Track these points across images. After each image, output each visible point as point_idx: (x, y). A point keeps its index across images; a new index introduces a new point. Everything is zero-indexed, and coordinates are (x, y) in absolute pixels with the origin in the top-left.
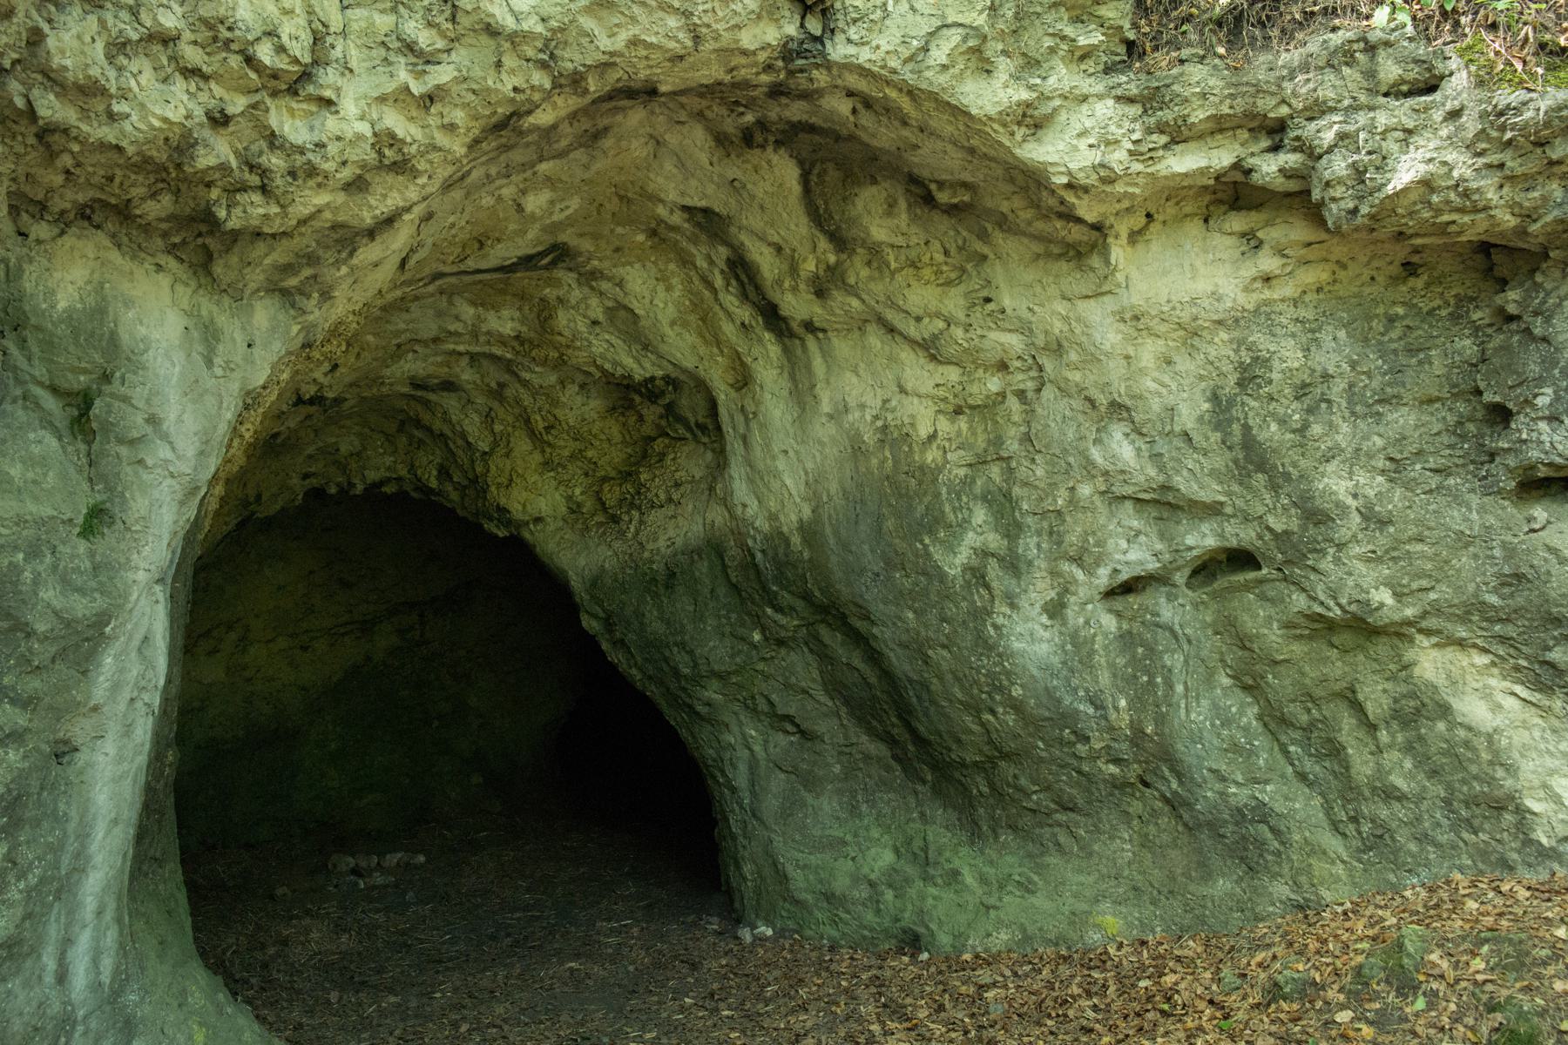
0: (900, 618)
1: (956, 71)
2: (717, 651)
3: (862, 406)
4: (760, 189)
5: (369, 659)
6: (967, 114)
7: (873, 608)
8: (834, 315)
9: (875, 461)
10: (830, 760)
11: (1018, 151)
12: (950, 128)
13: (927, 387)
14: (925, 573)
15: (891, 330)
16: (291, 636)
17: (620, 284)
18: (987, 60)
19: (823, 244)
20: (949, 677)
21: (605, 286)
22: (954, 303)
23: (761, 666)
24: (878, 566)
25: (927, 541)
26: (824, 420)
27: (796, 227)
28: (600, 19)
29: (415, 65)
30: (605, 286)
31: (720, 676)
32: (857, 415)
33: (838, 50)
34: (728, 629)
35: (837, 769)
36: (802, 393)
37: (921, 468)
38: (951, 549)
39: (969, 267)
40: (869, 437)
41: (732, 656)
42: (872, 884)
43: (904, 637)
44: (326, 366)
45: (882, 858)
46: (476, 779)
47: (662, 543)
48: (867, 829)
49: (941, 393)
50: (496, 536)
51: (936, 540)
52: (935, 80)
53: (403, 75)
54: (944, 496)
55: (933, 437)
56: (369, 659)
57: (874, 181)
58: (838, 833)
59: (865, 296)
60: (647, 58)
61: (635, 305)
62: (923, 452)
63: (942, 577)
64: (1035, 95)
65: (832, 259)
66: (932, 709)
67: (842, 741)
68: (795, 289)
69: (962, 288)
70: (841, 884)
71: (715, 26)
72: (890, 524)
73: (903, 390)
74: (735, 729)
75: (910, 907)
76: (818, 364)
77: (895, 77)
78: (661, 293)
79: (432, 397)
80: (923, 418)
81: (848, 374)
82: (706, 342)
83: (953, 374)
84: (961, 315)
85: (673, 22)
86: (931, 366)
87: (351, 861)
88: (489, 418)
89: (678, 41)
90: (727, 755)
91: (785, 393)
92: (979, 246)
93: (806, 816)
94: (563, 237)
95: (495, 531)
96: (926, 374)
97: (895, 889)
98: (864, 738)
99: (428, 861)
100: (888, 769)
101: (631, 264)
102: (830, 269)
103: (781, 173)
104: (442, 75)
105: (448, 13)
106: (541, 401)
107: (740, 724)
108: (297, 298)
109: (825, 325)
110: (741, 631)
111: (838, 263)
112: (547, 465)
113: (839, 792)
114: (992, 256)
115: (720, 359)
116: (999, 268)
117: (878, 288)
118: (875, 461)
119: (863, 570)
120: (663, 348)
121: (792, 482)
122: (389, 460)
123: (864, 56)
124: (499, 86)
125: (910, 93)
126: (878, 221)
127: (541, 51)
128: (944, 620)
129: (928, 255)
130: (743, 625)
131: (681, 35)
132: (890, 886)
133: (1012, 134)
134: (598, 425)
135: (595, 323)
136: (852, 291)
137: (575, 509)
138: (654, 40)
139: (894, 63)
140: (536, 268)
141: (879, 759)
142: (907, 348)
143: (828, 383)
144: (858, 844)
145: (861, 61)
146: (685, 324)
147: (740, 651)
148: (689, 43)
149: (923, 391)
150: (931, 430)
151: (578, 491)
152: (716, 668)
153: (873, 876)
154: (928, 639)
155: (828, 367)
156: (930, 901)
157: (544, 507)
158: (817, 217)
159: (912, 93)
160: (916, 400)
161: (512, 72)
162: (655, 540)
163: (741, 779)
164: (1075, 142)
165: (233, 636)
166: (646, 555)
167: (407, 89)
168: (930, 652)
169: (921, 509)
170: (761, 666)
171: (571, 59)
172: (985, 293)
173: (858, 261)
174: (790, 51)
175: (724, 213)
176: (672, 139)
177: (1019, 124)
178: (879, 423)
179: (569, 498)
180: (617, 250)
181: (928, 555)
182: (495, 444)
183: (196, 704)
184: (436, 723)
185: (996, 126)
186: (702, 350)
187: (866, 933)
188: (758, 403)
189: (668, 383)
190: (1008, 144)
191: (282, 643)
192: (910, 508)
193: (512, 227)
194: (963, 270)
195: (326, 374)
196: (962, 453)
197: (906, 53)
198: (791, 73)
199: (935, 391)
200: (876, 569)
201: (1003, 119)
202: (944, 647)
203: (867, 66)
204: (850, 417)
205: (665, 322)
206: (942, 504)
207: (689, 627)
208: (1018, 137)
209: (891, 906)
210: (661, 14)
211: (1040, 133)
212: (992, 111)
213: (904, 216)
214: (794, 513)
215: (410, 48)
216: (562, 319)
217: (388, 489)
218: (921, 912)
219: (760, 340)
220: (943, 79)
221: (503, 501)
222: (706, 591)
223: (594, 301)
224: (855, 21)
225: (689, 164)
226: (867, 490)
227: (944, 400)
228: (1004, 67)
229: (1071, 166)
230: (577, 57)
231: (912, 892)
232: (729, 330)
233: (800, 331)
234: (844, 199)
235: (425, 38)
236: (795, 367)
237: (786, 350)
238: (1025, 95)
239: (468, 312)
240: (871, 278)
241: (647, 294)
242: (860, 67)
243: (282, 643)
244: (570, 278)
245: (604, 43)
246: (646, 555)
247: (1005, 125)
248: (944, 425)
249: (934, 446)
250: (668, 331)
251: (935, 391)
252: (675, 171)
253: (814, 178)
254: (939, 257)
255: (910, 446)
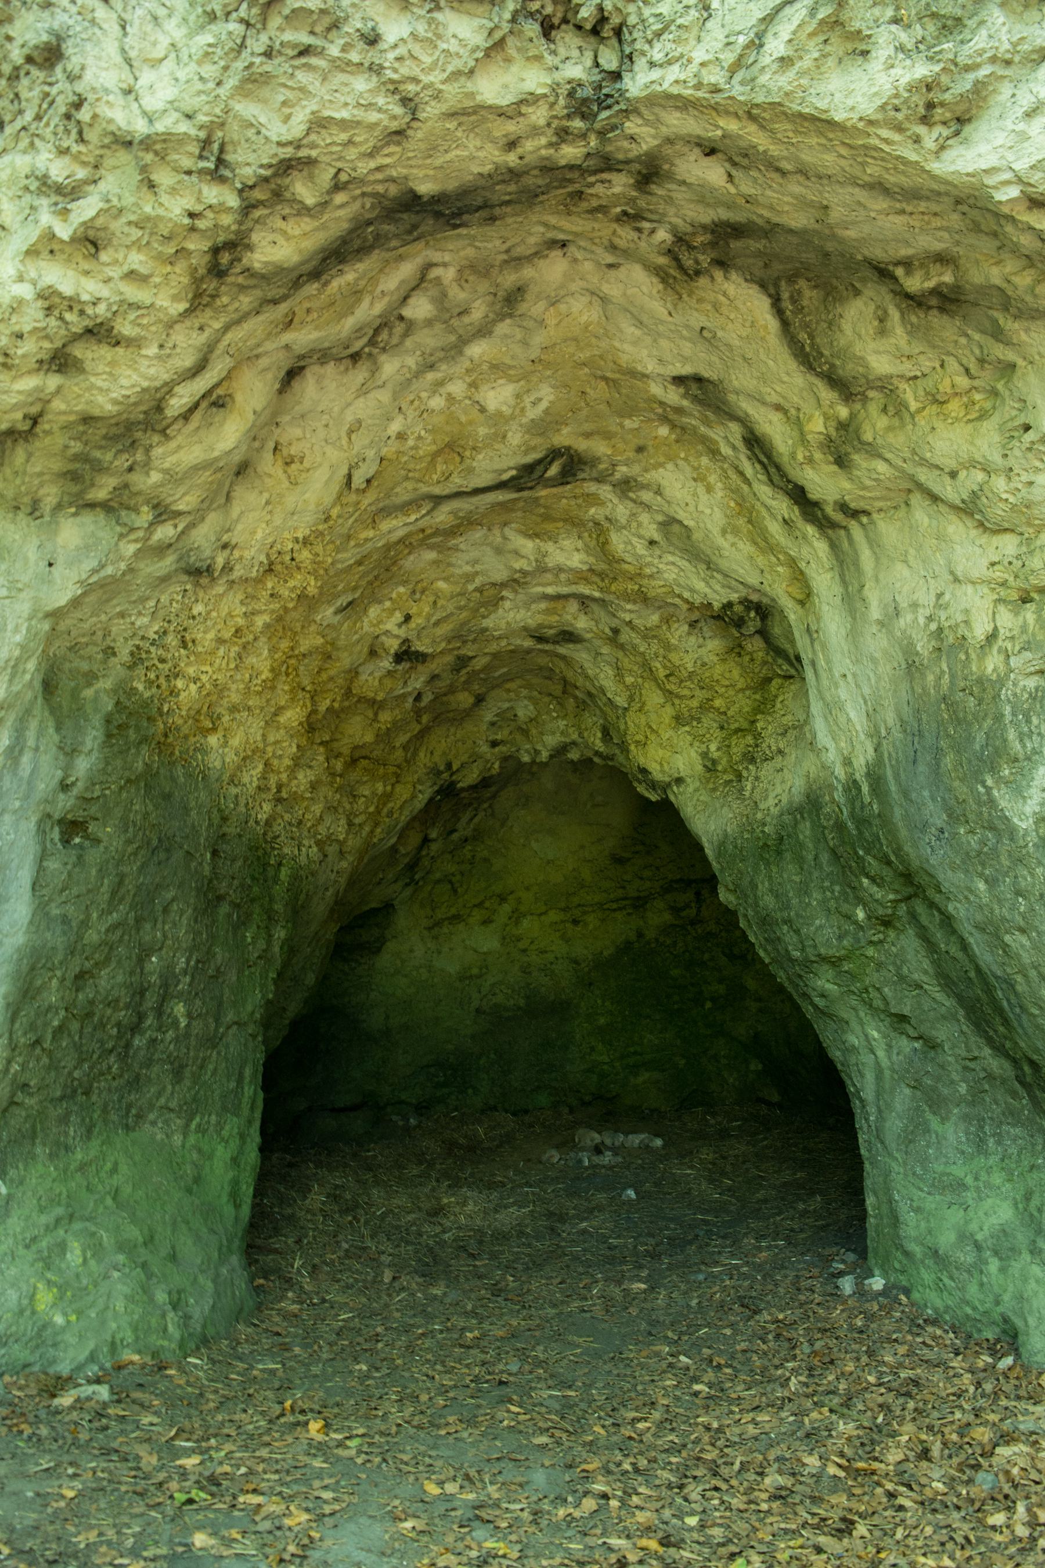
0: (971, 891)
1: (807, 63)
2: (823, 931)
3: (915, 606)
4: (732, 334)
5: (640, 935)
6: (831, 123)
7: (941, 877)
8: (865, 488)
9: (930, 678)
10: (955, 1076)
11: (936, 167)
12: (829, 158)
13: (979, 569)
14: (992, 828)
15: (935, 498)
16: (564, 910)
17: (659, 492)
18: (857, 35)
19: (827, 395)
20: (1033, 974)
21: (646, 496)
22: (987, 442)
23: (870, 952)
24: (940, 819)
25: (989, 782)
26: (874, 629)
27: (790, 380)
28: (265, 101)
29: (56, 204)
30: (646, 496)
31: (834, 962)
32: (909, 617)
33: (637, 83)
34: (832, 904)
35: (963, 1088)
36: (852, 601)
37: (980, 681)
38: (1019, 793)
39: (1000, 386)
40: (923, 647)
41: (840, 938)
42: (978, 1246)
43: (979, 917)
44: (398, 617)
45: (997, 1213)
46: (755, 1066)
47: (771, 801)
48: (989, 1171)
49: (998, 574)
50: (647, 800)
51: (999, 780)
52: (773, 84)
53: (46, 218)
54: (1008, 718)
55: (992, 637)
56: (640, 935)
57: (857, 293)
58: (958, 1171)
59: (888, 456)
60: (350, 142)
61: (681, 515)
62: (981, 658)
63: (1012, 832)
64: (937, 68)
65: (843, 412)
66: (1024, 1017)
67: (964, 1054)
68: (810, 460)
69: (996, 419)
70: (946, 1239)
71: (426, 79)
72: (948, 761)
73: (957, 580)
74: (857, 1028)
75: (1011, 1288)
76: (866, 557)
77: (718, 98)
78: (704, 497)
79: (561, 650)
80: (979, 612)
81: (899, 566)
82: (762, 551)
83: (1009, 545)
84: (996, 458)
85: (361, 84)
86: (984, 539)
87: (597, 1137)
88: (619, 674)
89: (380, 110)
90: (853, 1060)
91: (838, 600)
92: (1000, 352)
93: (928, 1146)
94: (564, 437)
95: (647, 794)
96: (979, 551)
97: (1001, 1259)
98: (987, 1051)
99: (664, 1147)
100: (1014, 1094)
101: (662, 465)
102: (843, 426)
103: (742, 308)
104: (86, 209)
105: (74, 134)
106: (655, 646)
107: (862, 1024)
108: (123, 513)
109: (862, 505)
110: (845, 908)
111: (853, 416)
112: (679, 720)
113: (966, 1118)
114: (1020, 362)
115: (780, 569)
116: (1033, 379)
117: (898, 440)
118: (930, 678)
119: (926, 825)
120: (724, 564)
121: (855, 715)
122: (562, 723)
123: (670, 78)
124: (161, 212)
125: (752, 117)
126: (872, 345)
127: (201, 157)
128: (1018, 893)
129: (947, 382)
130: (846, 900)
131: (381, 101)
132: (996, 1253)
133: (917, 140)
134: (718, 669)
135: (652, 543)
136: (873, 451)
137: (711, 767)
138: (344, 114)
139: (715, 76)
140: (542, 481)
141: (1004, 1082)
142: (953, 518)
143: (877, 580)
144: (978, 1189)
145: (666, 86)
146: (736, 531)
147: (847, 932)
148: (398, 110)
149: (975, 574)
150: (990, 628)
151: (713, 747)
152: (823, 951)
153: (979, 1237)
154: (1004, 919)
155: (877, 560)
156: (1032, 1285)
157: (682, 767)
158: (807, 358)
159: (751, 114)
160: (970, 589)
161: (173, 191)
162: (766, 798)
163: (868, 1093)
164: (1021, 126)
165: (507, 908)
166: (759, 816)
167: (50, 236)
168: (1007, 938)
169: (980, 738)
170: (870, 952)
171: (249, 162)
172: (1021, 420)
173: (873, 408)
174: (585, 101)
175: (715, 377)
176: (612, 289)
177: (925, 120)
178: (933, 626)
179: (705, 755)
180: (640, 449)
181: (992, 802)
182: (631, 699)
183: (475, 971)
184: (708, 1005)
185: (885, 133)
186: (761, 561)
187: (969, 1310)
188: (818, 620)
189: (748, 609)
190: (913, 157)
191: (553, 916)
192: (970, 739)
193: (482, 431)
194: (994, 393)
195: (400, 625)
196: (1028, 655)
197: (729, 57)
198: (601, 134)
199: (990, 573)
200: (939, 823)
201: (892, 114)
202: (1023, 931)
203: (675, 90)
204: (902, 621)
205: (716, 531)
206: (1004, 729)
207: (795, 901)
208: (929, 142)
209: (994, 1282)
210: (342, 77)
211: (967, 129)
212: (868, 108)
213: (899, 331)
214: (863, 756)
215: (45, 185)
216: (618, 542)
217: (574, 755)
218: (1020, 1298)
219: (805, 537)
220: (785, 81)
221: (642, 761)
222: (810, 857)
223: (644, 518)
224: (658, 35)
225: (645, 318)
226: (924, 717)
227: (1004, 584)
228: (885, 39)
229: (1016, 166)
230: (251, 158)
231: (1016, 1267)
232: (774, 528)
233: (838, 517)
234: (830, 324)
235: (59, 170)
236: (844, 563)
237: (834, 546)
238: (922, 70)
239: (528, 546)
240: (890, 429)
241: (689, 499)
242: (668, 96)
243: (553, 916)
244: (605, 491)
245: (277, 130)
246: (759, 816)
247: (899, 128)
248: (1006, 620)
249: (995, 649)
250: (720, 541)
251: (990, 573)
252: (638, 332)
253: (787, 305)
254: (963, 382)
255: (967, 653)
